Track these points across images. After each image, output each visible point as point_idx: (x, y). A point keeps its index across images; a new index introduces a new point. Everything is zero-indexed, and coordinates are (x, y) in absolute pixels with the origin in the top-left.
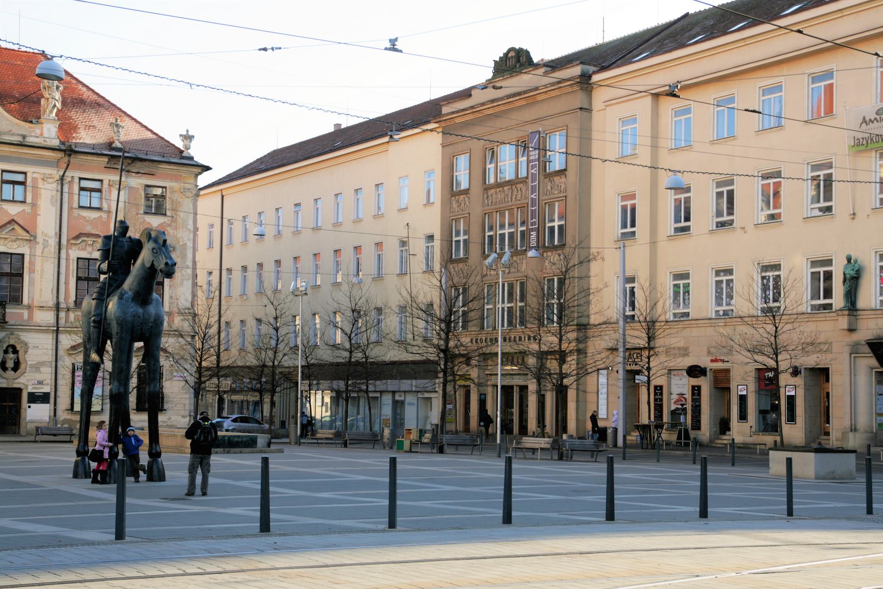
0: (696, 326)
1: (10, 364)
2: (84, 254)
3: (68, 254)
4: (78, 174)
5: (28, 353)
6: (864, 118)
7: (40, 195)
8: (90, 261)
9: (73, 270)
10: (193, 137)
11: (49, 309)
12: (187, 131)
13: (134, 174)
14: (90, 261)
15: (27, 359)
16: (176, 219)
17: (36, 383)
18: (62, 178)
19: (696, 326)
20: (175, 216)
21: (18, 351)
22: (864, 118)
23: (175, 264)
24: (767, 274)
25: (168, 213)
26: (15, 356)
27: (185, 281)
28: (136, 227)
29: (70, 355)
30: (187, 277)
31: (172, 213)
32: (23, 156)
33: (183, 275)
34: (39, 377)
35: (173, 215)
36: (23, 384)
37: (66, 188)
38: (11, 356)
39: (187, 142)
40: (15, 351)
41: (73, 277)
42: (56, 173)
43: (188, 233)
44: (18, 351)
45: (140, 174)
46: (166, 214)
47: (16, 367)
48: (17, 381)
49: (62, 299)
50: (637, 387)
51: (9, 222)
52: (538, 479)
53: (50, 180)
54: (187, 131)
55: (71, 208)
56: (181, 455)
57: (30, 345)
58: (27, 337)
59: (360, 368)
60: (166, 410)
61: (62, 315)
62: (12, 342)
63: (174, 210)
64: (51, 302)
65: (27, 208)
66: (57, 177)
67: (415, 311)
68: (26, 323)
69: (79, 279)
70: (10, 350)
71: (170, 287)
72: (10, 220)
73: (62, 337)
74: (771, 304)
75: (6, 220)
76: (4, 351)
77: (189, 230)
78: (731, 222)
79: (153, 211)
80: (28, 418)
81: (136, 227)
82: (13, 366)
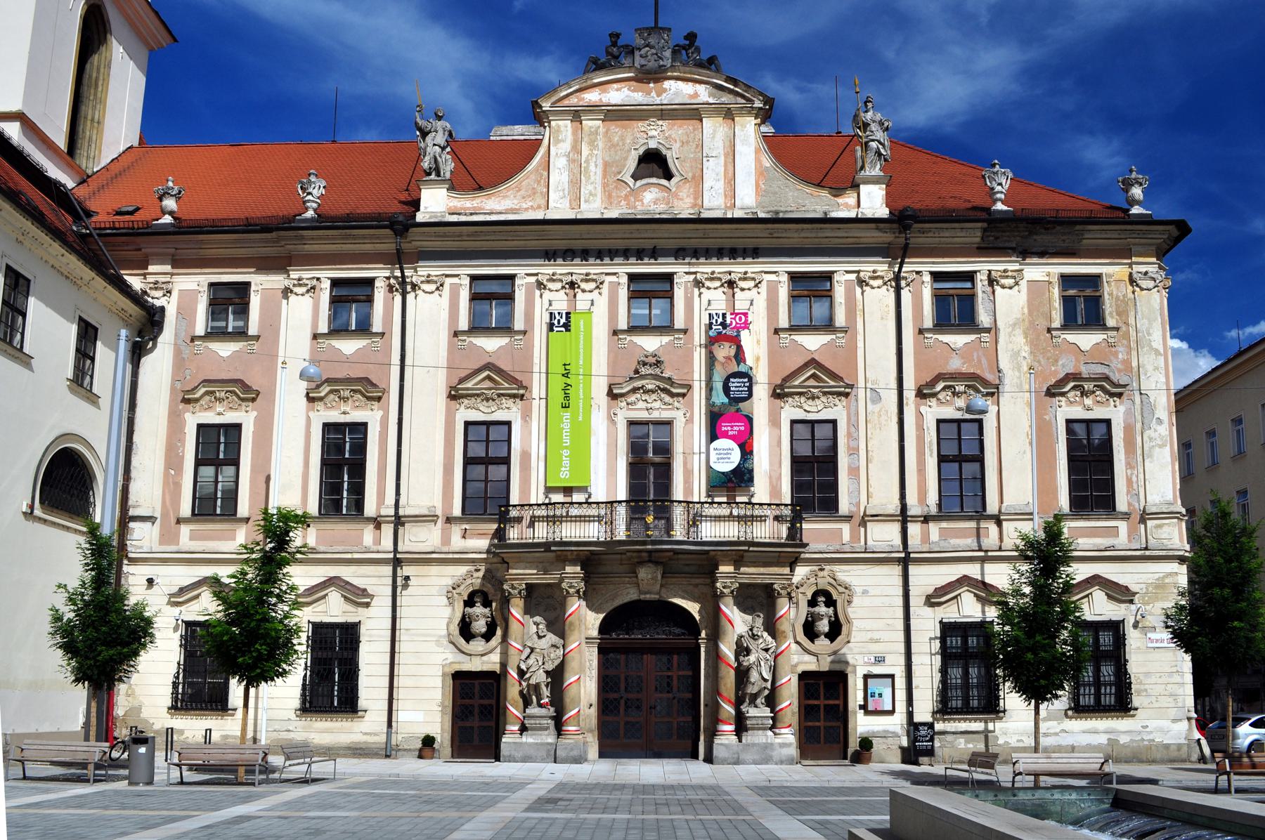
0: (721, 452)
2: (949, 412)
3: (920, 415)
5: (853, 605)
8: (963, 425)
14: (963, 425)
15: (851, 615)
17: (873, 660)
18: (897, 278)
19: (721, 452)
20: (1124, 328)
21: (836, 601)
23: (987, 412)
26: (831, 610)
28: (1049, 355)
29: (932, 605)
31: (1117, 322)
37: (906, 295)
38: (822, 609)
40: (830, 602)
41: (931, 455)
44: (836, 601)
49: (912, 499)
51: (806, 365)
56: (123, 812)
57: (858, 590)
58: (848, 574)
60: (1136, 709)
62: (823, 584)
64: (893, 506)
65: (841, 339)
66: (891, 275)
68: (847, 548)
69: (942, 459)
75: (801, 362)
76: (465, 602)
79: (1080, 323)
82: (484, 630)
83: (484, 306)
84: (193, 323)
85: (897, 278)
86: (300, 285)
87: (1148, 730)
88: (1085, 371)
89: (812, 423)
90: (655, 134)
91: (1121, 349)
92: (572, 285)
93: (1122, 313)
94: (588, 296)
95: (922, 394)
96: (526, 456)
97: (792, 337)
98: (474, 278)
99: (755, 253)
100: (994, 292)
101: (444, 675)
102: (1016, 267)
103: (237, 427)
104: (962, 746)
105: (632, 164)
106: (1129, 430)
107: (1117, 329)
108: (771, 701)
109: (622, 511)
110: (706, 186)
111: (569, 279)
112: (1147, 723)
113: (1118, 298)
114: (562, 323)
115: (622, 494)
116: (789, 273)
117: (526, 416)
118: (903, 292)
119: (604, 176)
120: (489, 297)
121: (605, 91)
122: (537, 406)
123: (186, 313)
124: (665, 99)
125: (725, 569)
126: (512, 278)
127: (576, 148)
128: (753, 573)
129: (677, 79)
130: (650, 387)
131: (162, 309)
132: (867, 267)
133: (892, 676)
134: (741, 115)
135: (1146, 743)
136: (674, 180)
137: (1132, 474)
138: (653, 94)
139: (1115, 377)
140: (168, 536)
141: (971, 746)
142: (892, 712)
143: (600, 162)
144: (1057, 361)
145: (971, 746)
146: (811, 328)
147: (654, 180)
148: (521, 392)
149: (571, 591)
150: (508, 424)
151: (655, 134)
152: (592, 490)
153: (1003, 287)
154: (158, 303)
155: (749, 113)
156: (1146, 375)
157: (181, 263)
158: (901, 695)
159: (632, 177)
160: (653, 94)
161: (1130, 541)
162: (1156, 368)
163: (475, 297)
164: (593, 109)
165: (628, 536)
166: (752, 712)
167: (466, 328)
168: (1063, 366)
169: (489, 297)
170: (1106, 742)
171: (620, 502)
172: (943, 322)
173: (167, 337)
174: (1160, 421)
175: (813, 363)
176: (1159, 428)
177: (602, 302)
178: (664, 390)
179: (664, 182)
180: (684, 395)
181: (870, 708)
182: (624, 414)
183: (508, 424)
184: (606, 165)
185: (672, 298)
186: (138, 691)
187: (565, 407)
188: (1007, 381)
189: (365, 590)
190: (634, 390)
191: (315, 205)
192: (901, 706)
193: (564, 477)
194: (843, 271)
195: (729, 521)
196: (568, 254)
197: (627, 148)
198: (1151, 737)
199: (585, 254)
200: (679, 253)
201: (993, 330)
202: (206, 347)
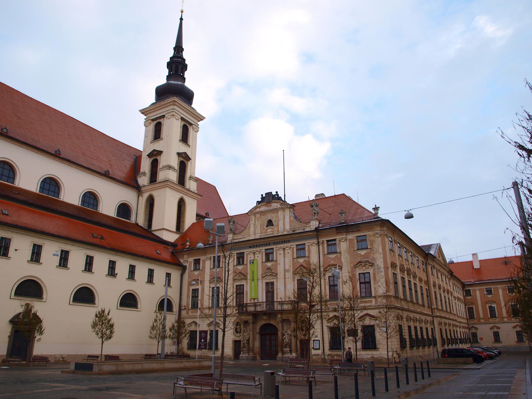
4: (325, 239)
7: (311, 252)
8: (365, 274)
9: (327, 282)
10: (379, 207)
12: (376, 206)
13: (350, 233)
14: (365, 274)
16: (373, 249)
18: (318, 243)
20: (372, 248)
24: (188, 263)
28: (354, 257)
30: (382, 277)
33: (380, 277)
35: (371, 247)
37: (321, 247)
39: (376, 211)
41: (327, 285)
42: (315, 241)
43: (380, 255)
45: (353, 232)
46: (368, 248)
50: (290, 381)
53: (314, 245)
54: (376, 206)
55: (324, 255)
60: (378, 348)
65: (306, 259)
67: (111, 329)
71: (374, 284)
77: (380, 253)
78: (316, 196)
81: (354, 257)
83: (330, 247)
84: (191, 268)
85: (318, 243)
86: (314, 243)
87: (382, 354)
88: (363, 260)
89: (364, 273)
90: (269, 216)
91: (372, 254)
92: (284, 249)
93: (372, 244)
94: (257, 255)
95: (325, 271)
96: (247, 292)
97: (298, 260)
98: (297, 245)
99: (289, 241)
100: (340, 243)
101: (232, 341)
102: (345, 236)
103: (198, 289)
104: (336, 358)
105: (266, 224)
106: (374, 275)
107: (371, 248)
108: (290, 347)
109: (265, 304)
110: (279, 227)
111: (254, 252)
112: (382, 352)
113: (370, 240)
114: (252, 262)
115: (264, 300)
116: (327, 240)
117: (247, 283)
118: (320, 246)
119: (260, 227)
120: (362, 241)
121: (260, 208)
122: (249, 281)
123: (190, 266)
124: (271, 208)
125: (279, 316)
126: (304, 244)
127: (255, 222)
128: (285, 317)
129: (274, 203)
130: (269, 275)
131: (186, 266)
132: (311, 241)
133: (319, 340)
134: (286, 209)
135: (381, 358)
136: (274, 226)
137: (375, 286)
138: (269, 207)
139: (370, 261)
140: (188, 313)
141: (337, 358)
142: (319, 349)
143: (259, 225)
144: (356, 258)
145: (337, 358)
146: (301, 257)
147: (270, 227)
148: (245, 278)
149: (250, 322)
150: (244, 285)
151: (269, 216)
152: (259, 299)
153: (342, 242)
154: (185, 265)
155: (288, 209)
156: (378, 260)
157: (189, 256)
158: (321, 345)
159: (273, 226)
160: (269, 207)
161: (375, 304)
162: (380, 258)
163: (297, 250)
164: (258, 212)
165: (266, 310)
166: (285, 349)
167: (265, 261)
168: (358, 260)
169: (362, 241)
170: (485, 361)
171: (264, 302)
172: (239, 264)
173: (187, 271)
174: (382, 271)
175: (302, 265)
176: (381, 273)
177: (260, 256)
178: (272, 275)
179: (272, 227)
180: (276, 276)
181: (314, 348)
182: (264, 281)
183: (244, 285)
184: (261, 225)
185: (273, 253)
186: (183, 346)
187: (253, 281)
188: (344, 265)
189: (219, 323)
190: (266, 275)
191: (211, 241)
192: (321, 348)
193: (253, 296)
194: (307, 242)
195: (255, 305)
196: (254, 246)
197: (265, 220)
198: (382, 356)
199: (257, 246)
200: (274, 244)
201: (340, 253)
202: (194, 273)
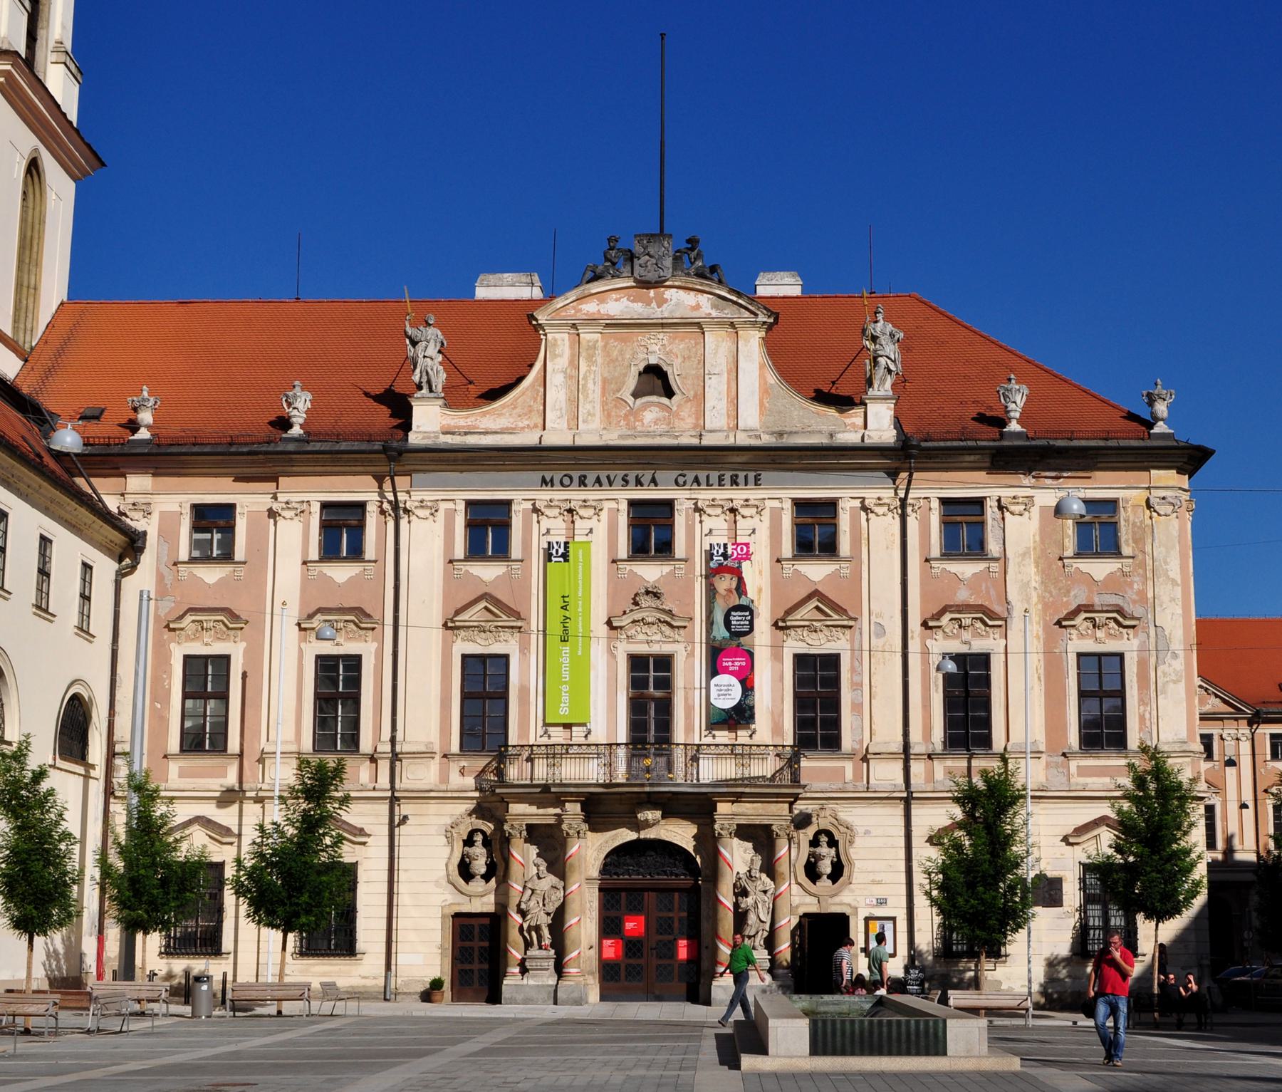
1: (826, 867)
6: (562, 608)
11: (891, 755)
17: (875, 902)
22: (562, 608)
25: (1126, 550)
26: (833, 851)
27: (1171, 685)
32: (826, 466)
34: (880, 891)
36: (849, 905)
37: (912, 522)
40: (833, 843)
44: (838, 841)
45: (1062, 480)
47: (837, 871)
48: (837, 900)
51: (809, 598)
52: (1220, 1036)
59: (197, 865)
61: (917, 768)
63: (1138, 541)
70: (824, 839)
72: (810, 591)
73: (916, 810)
74: (1029, 756)
75: (804, 593)
80: (613, 956)
